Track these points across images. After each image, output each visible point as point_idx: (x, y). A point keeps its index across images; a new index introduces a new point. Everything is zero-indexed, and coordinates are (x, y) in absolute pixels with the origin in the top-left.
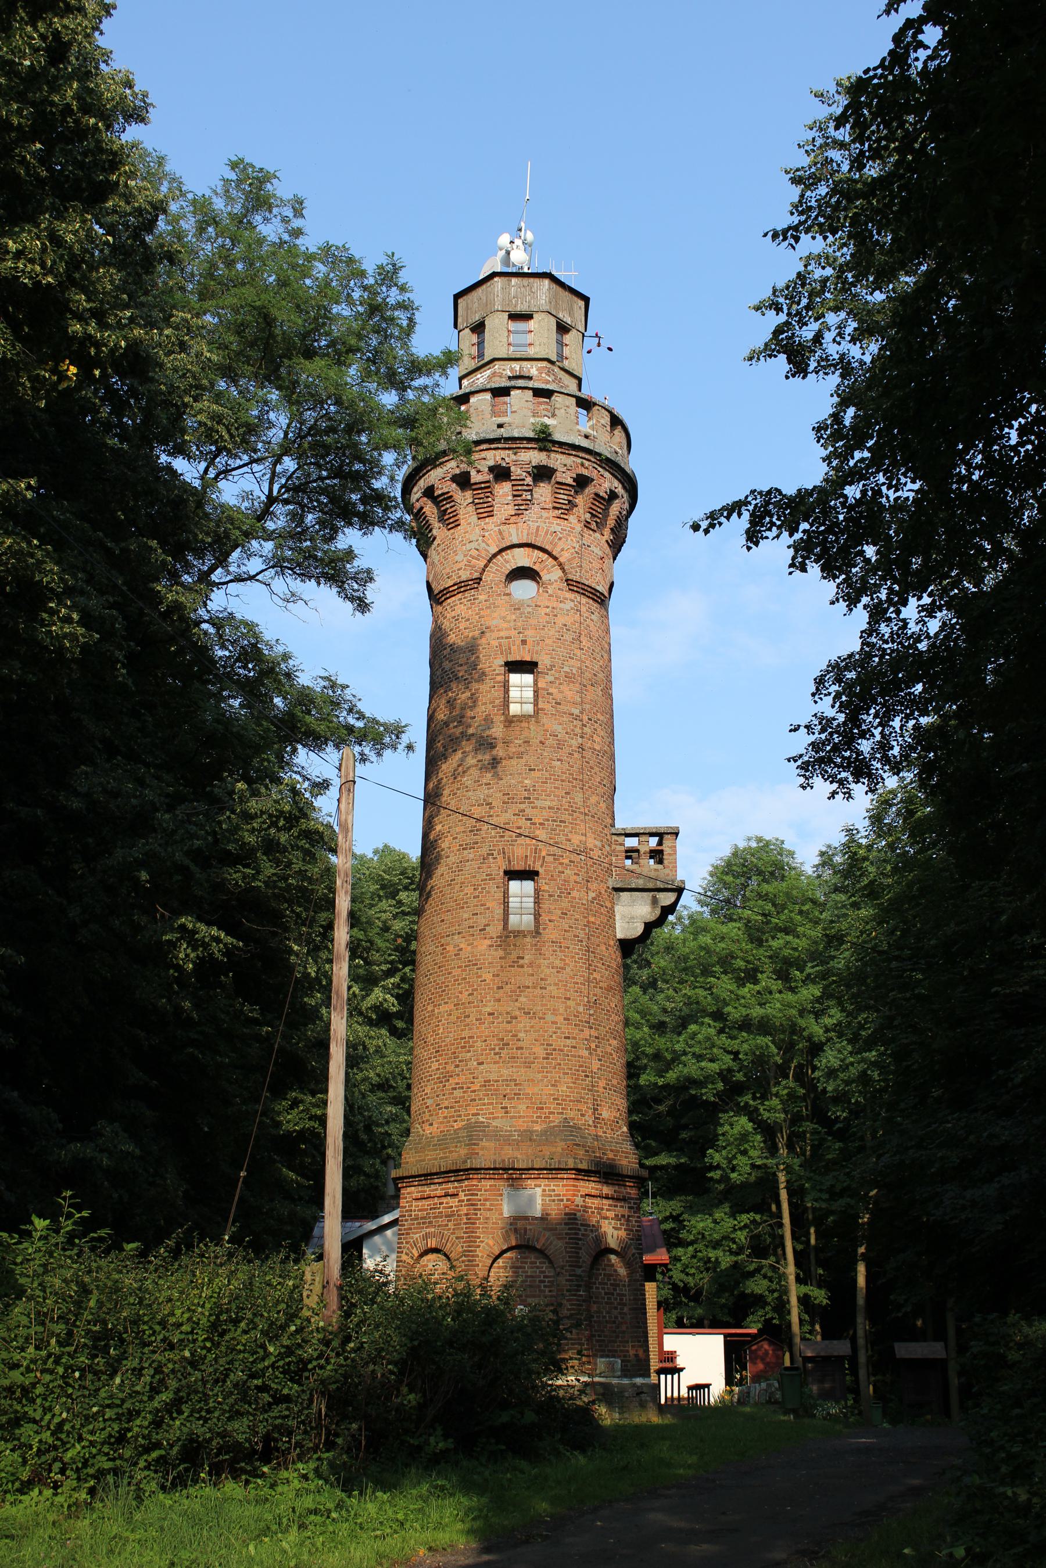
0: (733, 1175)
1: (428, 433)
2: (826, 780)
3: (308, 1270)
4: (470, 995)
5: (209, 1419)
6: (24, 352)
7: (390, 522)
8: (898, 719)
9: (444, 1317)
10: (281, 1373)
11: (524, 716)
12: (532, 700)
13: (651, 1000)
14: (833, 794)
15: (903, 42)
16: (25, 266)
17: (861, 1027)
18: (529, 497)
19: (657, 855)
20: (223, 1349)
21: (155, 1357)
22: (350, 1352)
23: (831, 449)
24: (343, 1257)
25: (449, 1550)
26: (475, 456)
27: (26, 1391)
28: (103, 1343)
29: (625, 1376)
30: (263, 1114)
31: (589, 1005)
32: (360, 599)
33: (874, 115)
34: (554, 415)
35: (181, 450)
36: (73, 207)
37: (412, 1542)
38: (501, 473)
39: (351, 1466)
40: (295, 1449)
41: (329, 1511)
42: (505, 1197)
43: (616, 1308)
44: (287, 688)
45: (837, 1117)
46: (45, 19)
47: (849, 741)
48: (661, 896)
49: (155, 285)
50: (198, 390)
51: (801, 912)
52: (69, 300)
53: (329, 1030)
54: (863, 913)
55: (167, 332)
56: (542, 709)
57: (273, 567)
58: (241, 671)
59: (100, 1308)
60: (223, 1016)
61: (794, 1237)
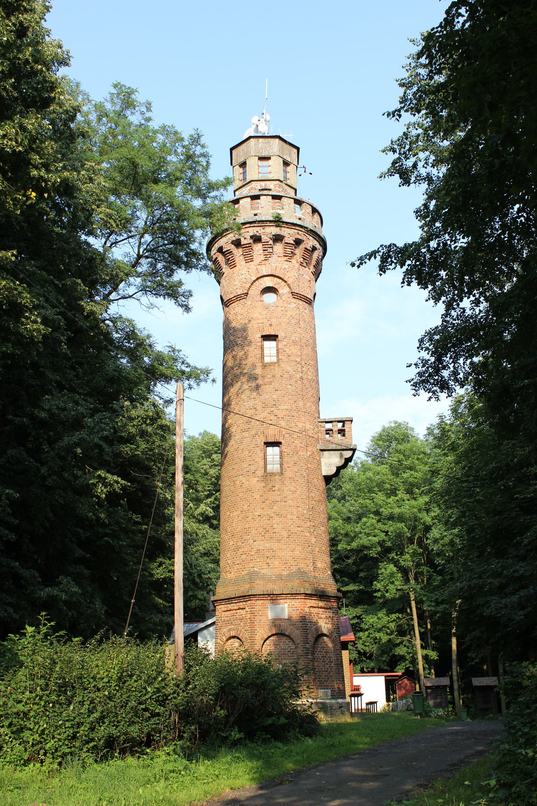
0: (387, 595)
1: (218, 220)
2: (426, 391)
3: (167, 649)
4: (248, 506)
5: (119, 726)
6: (9, 186)
7: (200, 266)
8: (462, 359)
9: (237, 671)
10: (155, 701)
11: (272, 363)
12: (276, 355)
13: (343, 506)
14: (430, 399)
15: (451, 13)
16: (8, 142)
17: (450, 517)
18: (271, 251)
19: (342, 432)
20: (125, 690)
21: (90, 695)
22: (189, 690)
23: (423, 222)
24: (185, 642)
25: (241, 789)
26: (243, 231)
27: (25, 714)
28: (64, 689)
29: (333, 698)
30: (143, 570)
31: (309, 510)
32: (186, 306)
33: (437, 52)
34: (283, 208)
35: (91, 233)
36: (31, 111)
37: (222, 785)
38: (257, 239)
39: (192, 748)
40: (163, 740)
41: (180, 771)
42: (269, 609)
43: (327, 664)
44: (150, 352)
45: (439, 563)
46: (15, 15)
47: (437, 371)
48: (344, 453)
49: (76, 149)
50: (99, 201)
51: (418, 459)
52: (30, 159)
53: (174, 527)
54: (449, 458)
55: (83, 173)
56: (281, 359)
57: (141, 291)
58: (127, 344)
59: (62, 671)
60: (122, 521)
61: (419, 625)
